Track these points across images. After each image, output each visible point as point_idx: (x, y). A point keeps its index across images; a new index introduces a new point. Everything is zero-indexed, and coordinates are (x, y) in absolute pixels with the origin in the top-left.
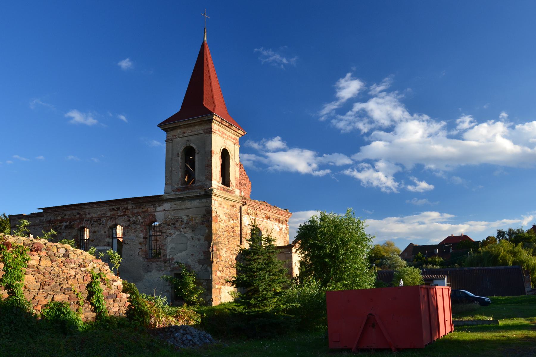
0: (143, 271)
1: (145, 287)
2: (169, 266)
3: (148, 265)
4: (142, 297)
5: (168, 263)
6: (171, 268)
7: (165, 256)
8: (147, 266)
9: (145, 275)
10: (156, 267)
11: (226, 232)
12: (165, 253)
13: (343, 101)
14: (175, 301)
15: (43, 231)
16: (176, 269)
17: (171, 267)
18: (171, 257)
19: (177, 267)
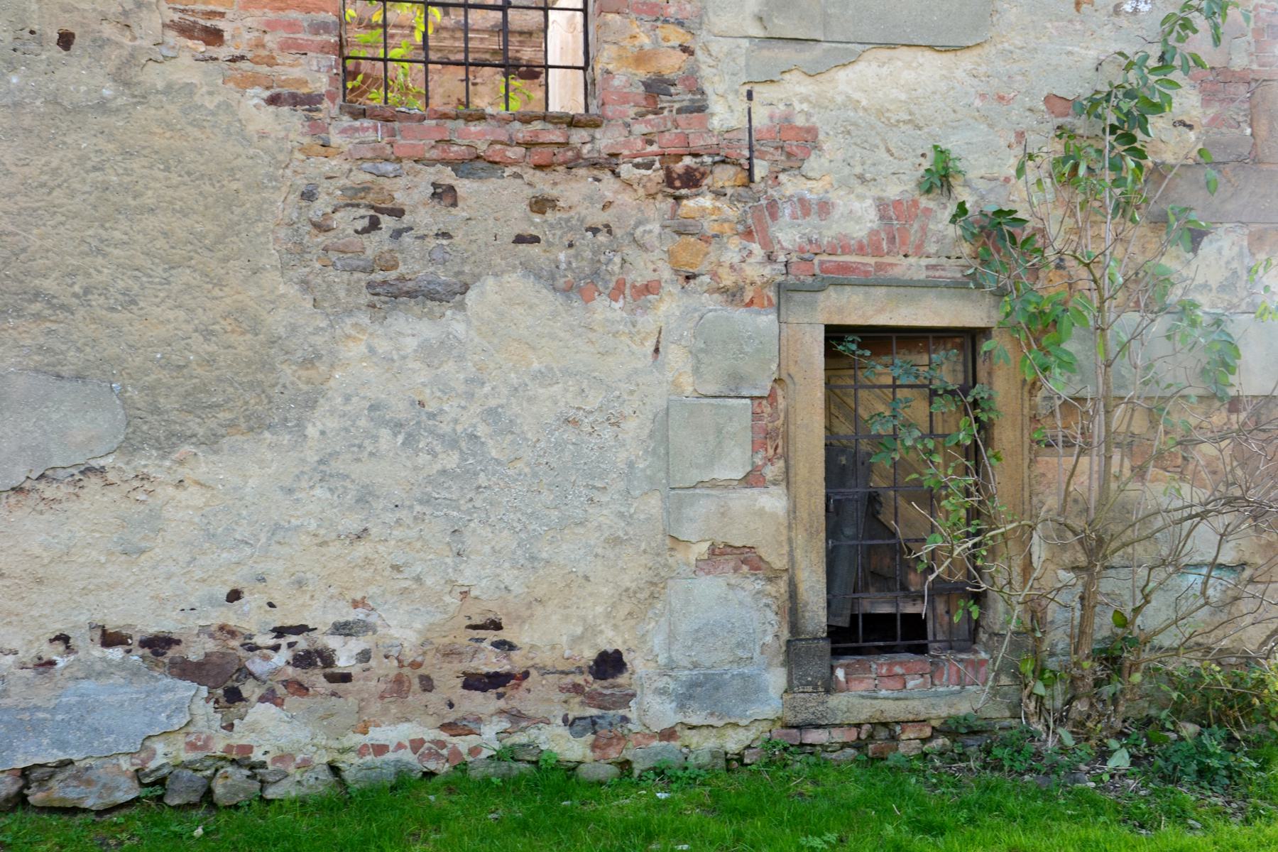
0: (305, 284)
1: (352, 523)
2: (748, 234)
3: (398, 213)
4: (1100, 309)
5: (719, 194)
6: (770, 258)
7: (682, 97)
8: (374, 225)
9: (355, 350)
10: (520, 239)
11: (1007, 180)
12: (672, 64)
13: (336, 671)
14: (840, 673)
15: (680, 847)
16: (844, 268)
17: (767, 243)
18: (761, 118)
19: (861, 250)
